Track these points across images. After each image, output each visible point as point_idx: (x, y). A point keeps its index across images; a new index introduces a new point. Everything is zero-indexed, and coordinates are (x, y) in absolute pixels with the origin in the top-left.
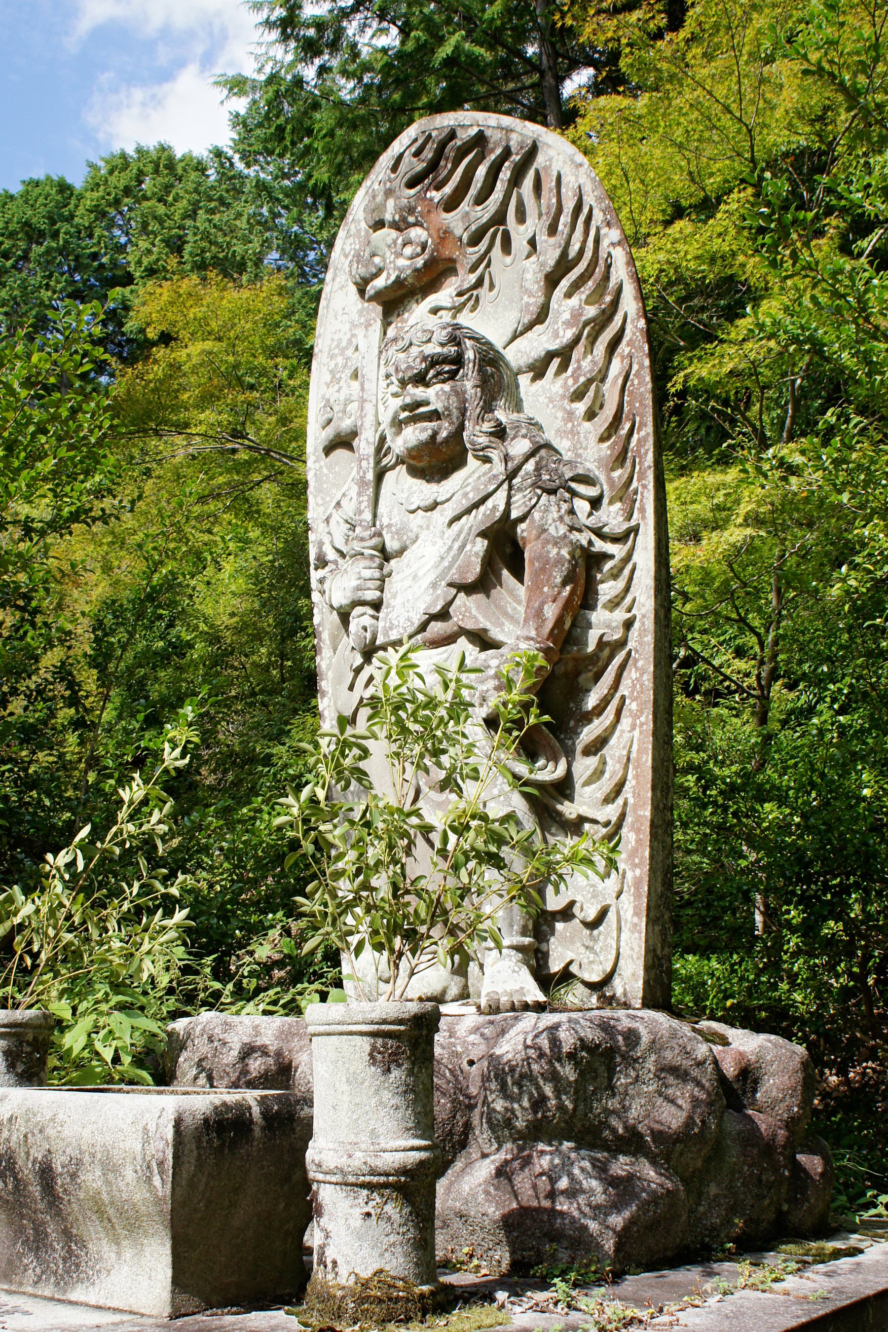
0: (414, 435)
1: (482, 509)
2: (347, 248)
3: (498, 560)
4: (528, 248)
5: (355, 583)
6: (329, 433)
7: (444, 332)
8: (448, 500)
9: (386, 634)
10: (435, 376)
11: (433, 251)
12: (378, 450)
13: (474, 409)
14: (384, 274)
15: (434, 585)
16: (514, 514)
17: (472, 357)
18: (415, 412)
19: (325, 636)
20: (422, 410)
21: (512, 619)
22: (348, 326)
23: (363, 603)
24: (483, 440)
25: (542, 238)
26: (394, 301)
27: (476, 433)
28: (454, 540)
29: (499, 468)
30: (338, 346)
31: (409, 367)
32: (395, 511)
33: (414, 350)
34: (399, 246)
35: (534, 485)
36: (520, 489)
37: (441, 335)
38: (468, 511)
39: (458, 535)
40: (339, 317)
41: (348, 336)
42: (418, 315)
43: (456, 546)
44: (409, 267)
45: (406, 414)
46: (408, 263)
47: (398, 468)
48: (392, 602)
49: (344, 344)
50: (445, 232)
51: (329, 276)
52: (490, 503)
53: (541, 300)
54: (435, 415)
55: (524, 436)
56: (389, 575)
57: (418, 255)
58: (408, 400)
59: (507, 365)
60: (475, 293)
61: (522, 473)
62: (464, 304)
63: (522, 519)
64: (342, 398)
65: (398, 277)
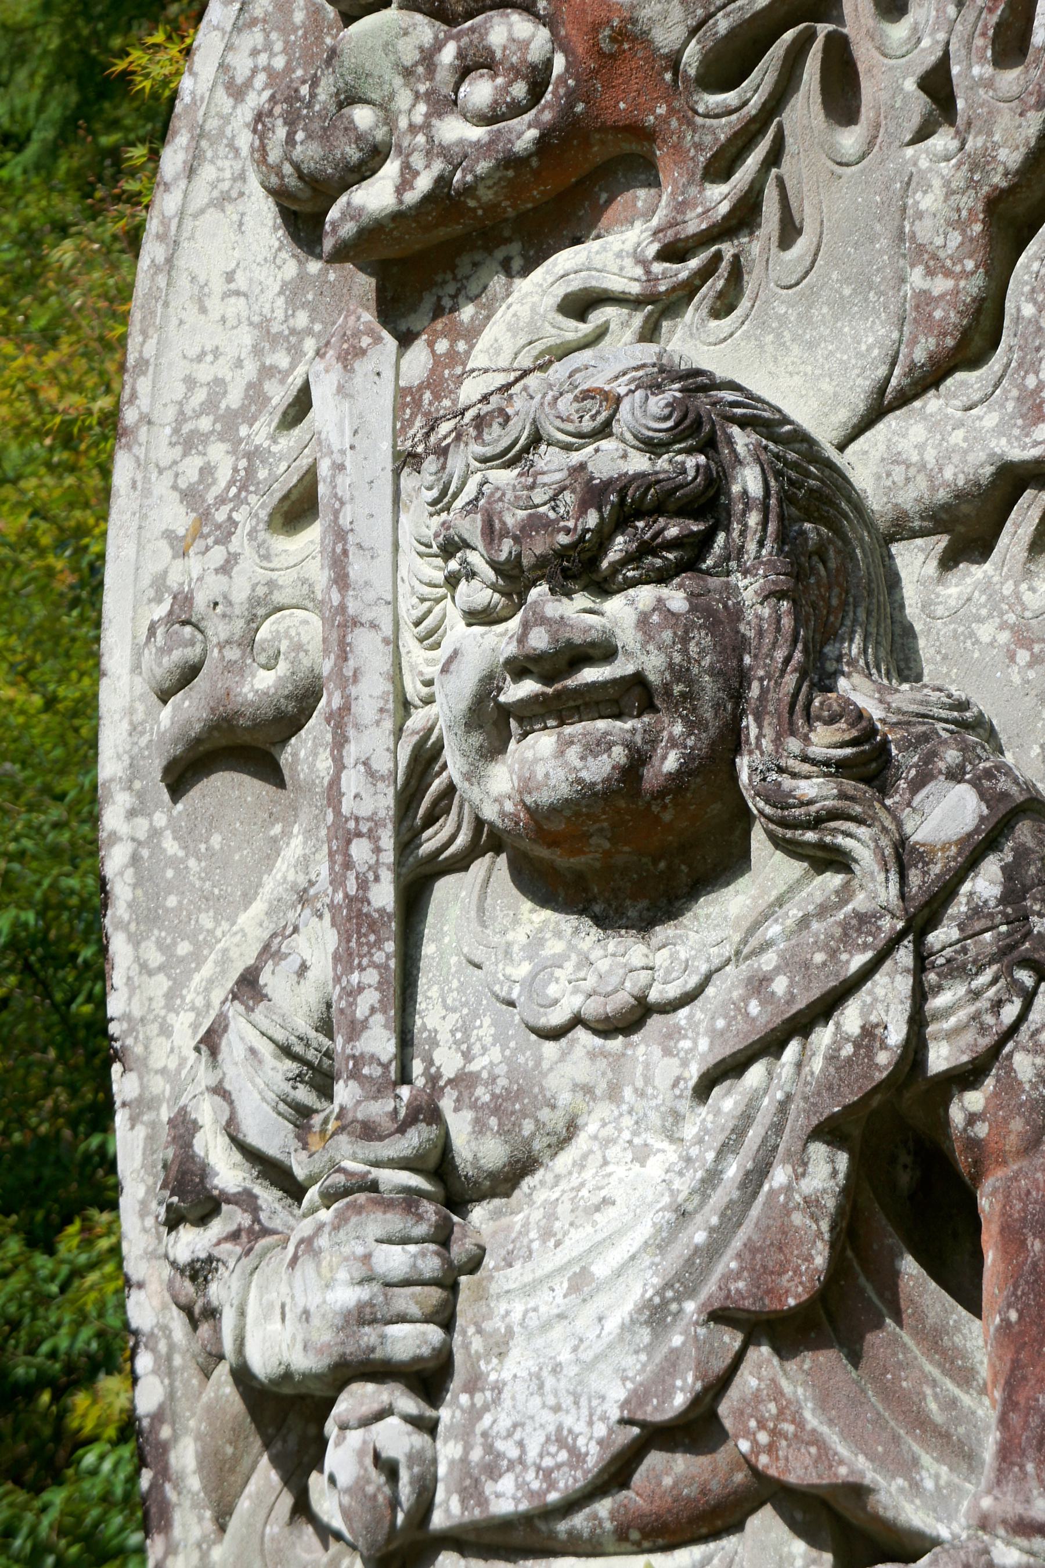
0: (548, 763)
1: (823, 1036)
2: (242, 65)
3: (881, 1220)
4: (919, 104)
5: (347, 1295)
6: (189, 709)
7: (657, 403)
8: (688, 998)
9: (471, 1491)
10: (631, 559)
11: (572, 97)
12: (408, 797)
13: (773, 671)
14: (391, 168)
15: (656, 1314)
16: (940, 1058)
17: (755, 489)
18: (561, 684)
19: (185, 1456)
20: (590, 674)
21: (961, 1454)
22: (246, 337)
23: (379, 1371)
24: (814, 789)
25: (971, 71)
26: (420, 269)
27: (786, 764)
28: (725, 1150)
29: (876, 890)
30: (210, 406)
31: (536, 524)
32: (485, 1029)
33: (552, 462)
34: (444, 76)
35: (1007, 955)
36: (956, 970)
37: (647, 411)
38: (770, 1045)
39: (739, 1132)
40: (214, 305)
41: (250, 370)
42: (517, 313)
43: (733, 1170)
44: (483, 148)
45: (529, 687)
46: (478, 133)
47: (479, 867)
48: (492, 1371)
49: (234, 399)
50: (620, 36)
51: (173, 158)
52: (851, 1017)
53: (973, 286)
54: (634, 695)
55: (955, 775)
56: (474, 1265)
57: (517, 110)
58: (539, 640)
59: (858, 506)
60: (728, 249)
61: (959, 907)
62: (688, 290)
63: (967, 1076)
64: (240, 594)
65: (442, 181)
